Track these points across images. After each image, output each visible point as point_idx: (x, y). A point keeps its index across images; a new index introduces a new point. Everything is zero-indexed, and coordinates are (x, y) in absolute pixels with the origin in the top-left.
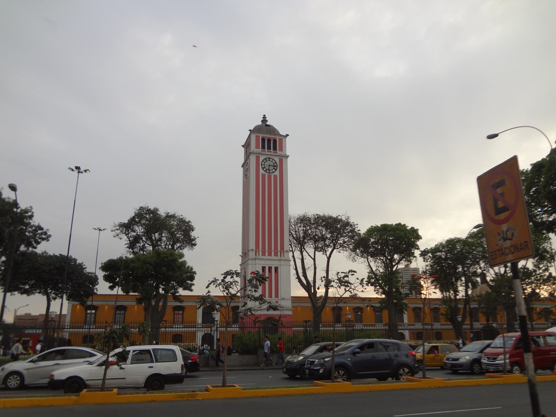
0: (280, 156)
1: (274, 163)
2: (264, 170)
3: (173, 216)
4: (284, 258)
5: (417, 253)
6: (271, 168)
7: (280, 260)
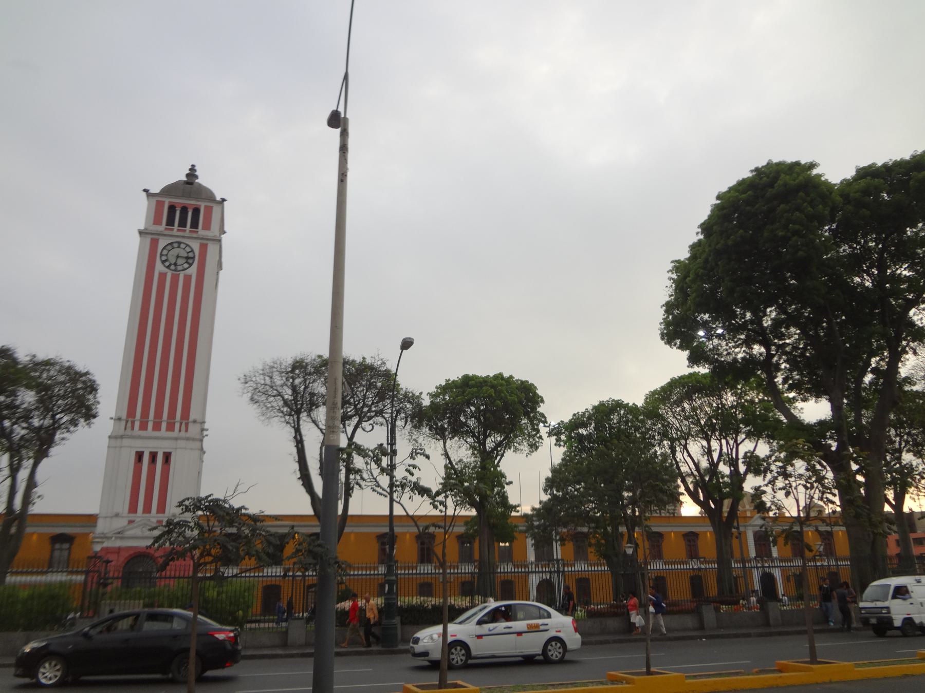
0: (202, 239)
2: (165, 266)
3: (48, 363)
4: (188, 435)
5: (543, 430)
7: (176, 439)
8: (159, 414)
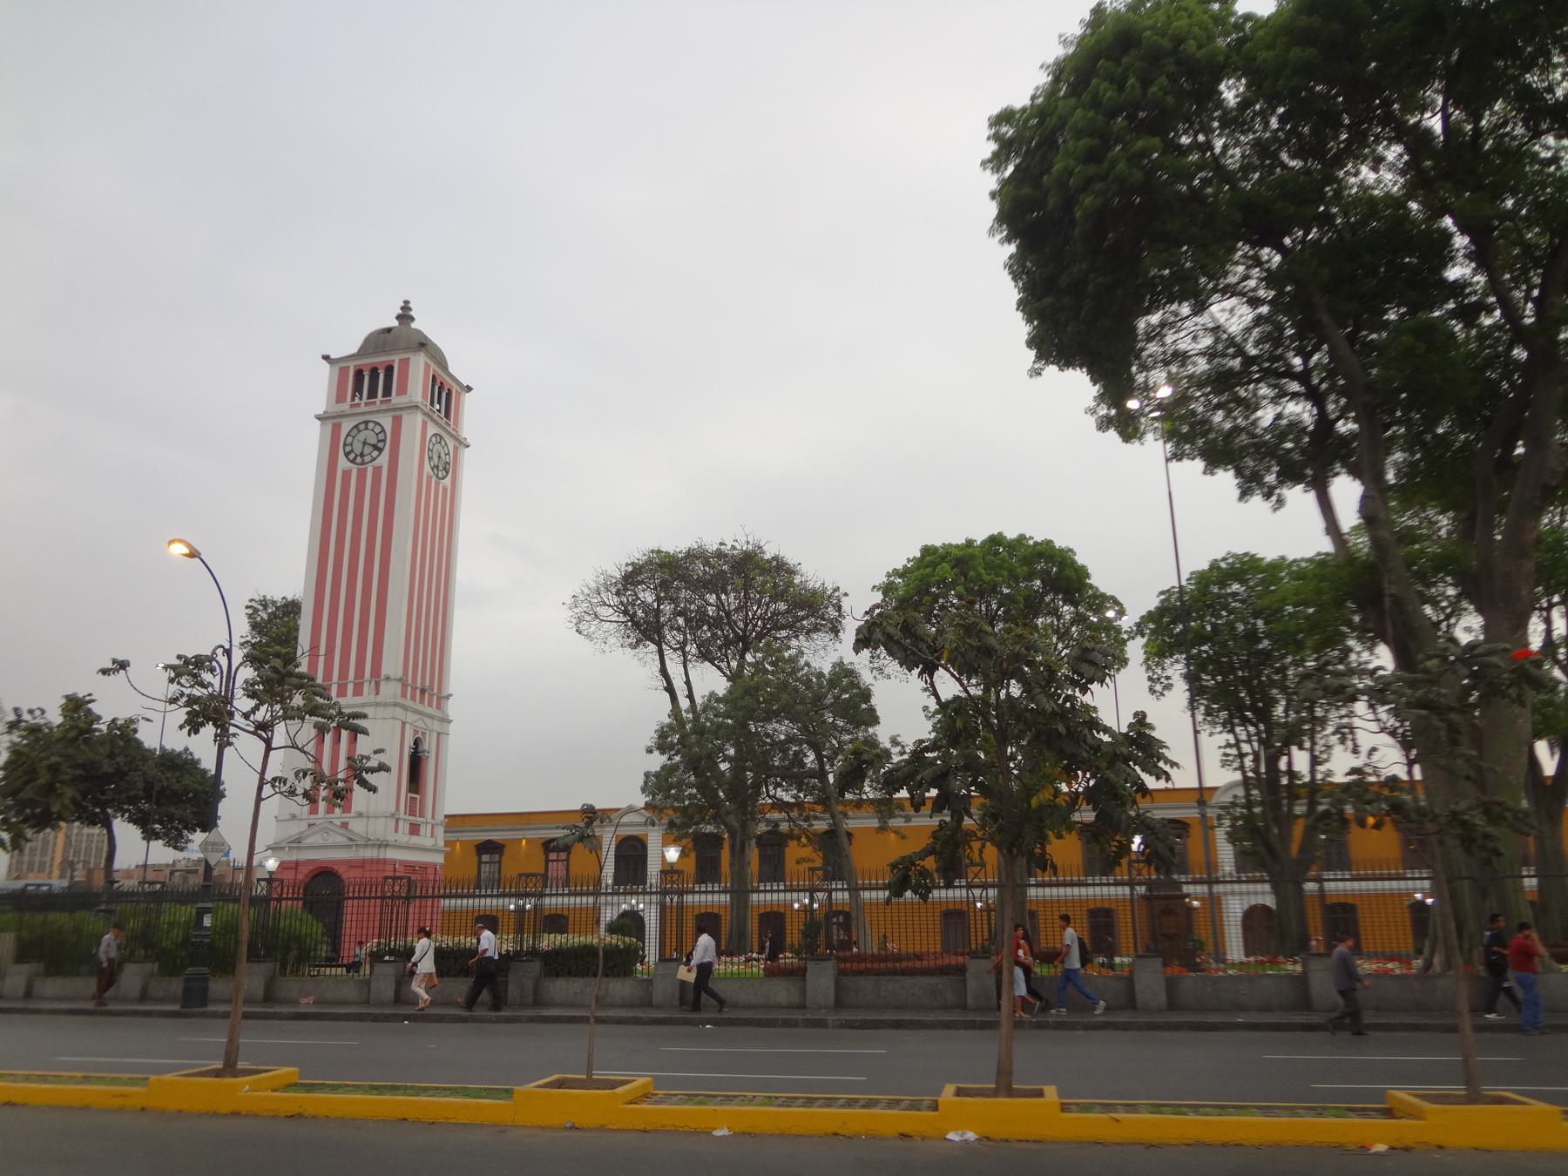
2: (348, 459)
6: (367, 449)
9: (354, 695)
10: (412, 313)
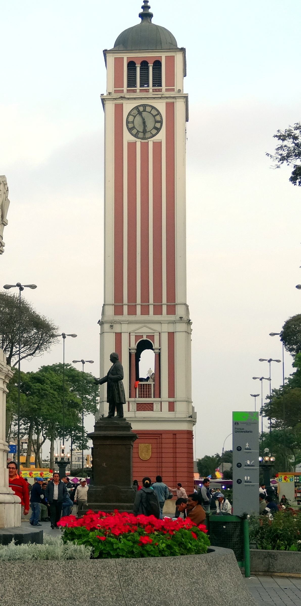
1: (135, 117)
2: (132, 134)
8: (145, 297)
9: (154, 314)
10: (150, 11)
